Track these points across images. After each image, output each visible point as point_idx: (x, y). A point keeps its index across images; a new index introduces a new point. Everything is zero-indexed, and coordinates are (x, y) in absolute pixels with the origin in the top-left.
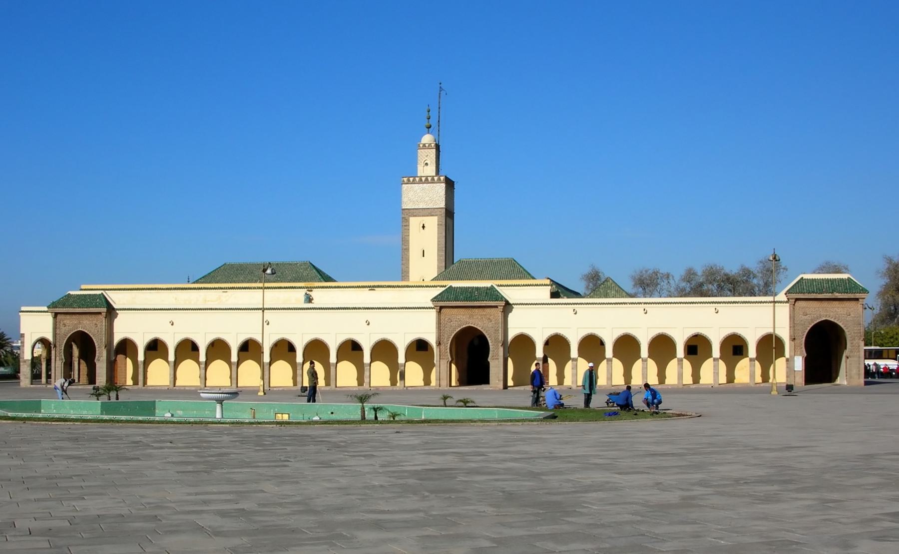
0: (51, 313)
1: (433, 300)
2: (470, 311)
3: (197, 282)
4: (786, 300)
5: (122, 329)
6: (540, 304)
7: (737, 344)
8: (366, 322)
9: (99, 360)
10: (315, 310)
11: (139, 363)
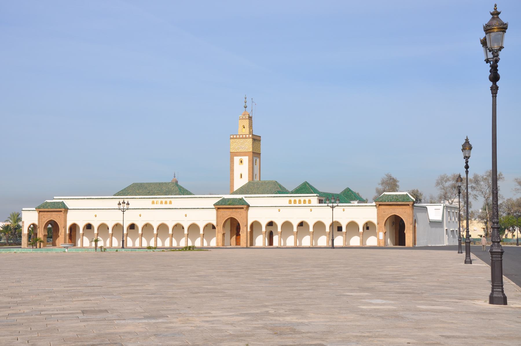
0: (37, 211)
1: (214, 205)
2: (231, 210)
3: (115, 195)
5: (71, 218)
6: (256, 207)
9: (61, 234)
10: (176, 210)
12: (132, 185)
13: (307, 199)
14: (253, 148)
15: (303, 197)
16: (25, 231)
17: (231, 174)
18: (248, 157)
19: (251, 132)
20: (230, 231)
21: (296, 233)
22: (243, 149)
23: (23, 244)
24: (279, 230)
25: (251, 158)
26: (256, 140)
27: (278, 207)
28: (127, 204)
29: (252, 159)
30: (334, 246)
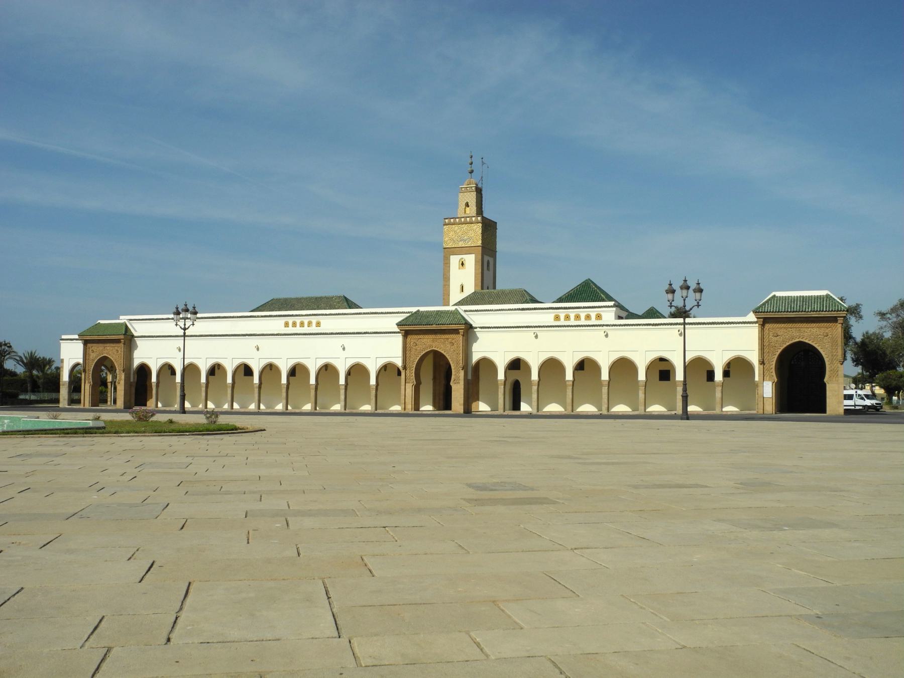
1: (399, 325)
3: (560, 300)
4: (756, 320)
7: (663, 367)
8: (342, 346)
11: (499, 382)
12: (270, 301)
13: (593, 313)
14: (483, 240)
15: (584, 310)
16: (65, 377)
17: (445, 286)
18: (473, 255)
19: (480, 211)
20: (433, 379)
21: (571, 383)
22: (466, 242)
23: (61, 400)
24: (535, 376)
25: (480, 257)
26: (489, 228)
27: (533, 329)
28: (695, 291)
29: (480, 258)
30: (186, 410)
